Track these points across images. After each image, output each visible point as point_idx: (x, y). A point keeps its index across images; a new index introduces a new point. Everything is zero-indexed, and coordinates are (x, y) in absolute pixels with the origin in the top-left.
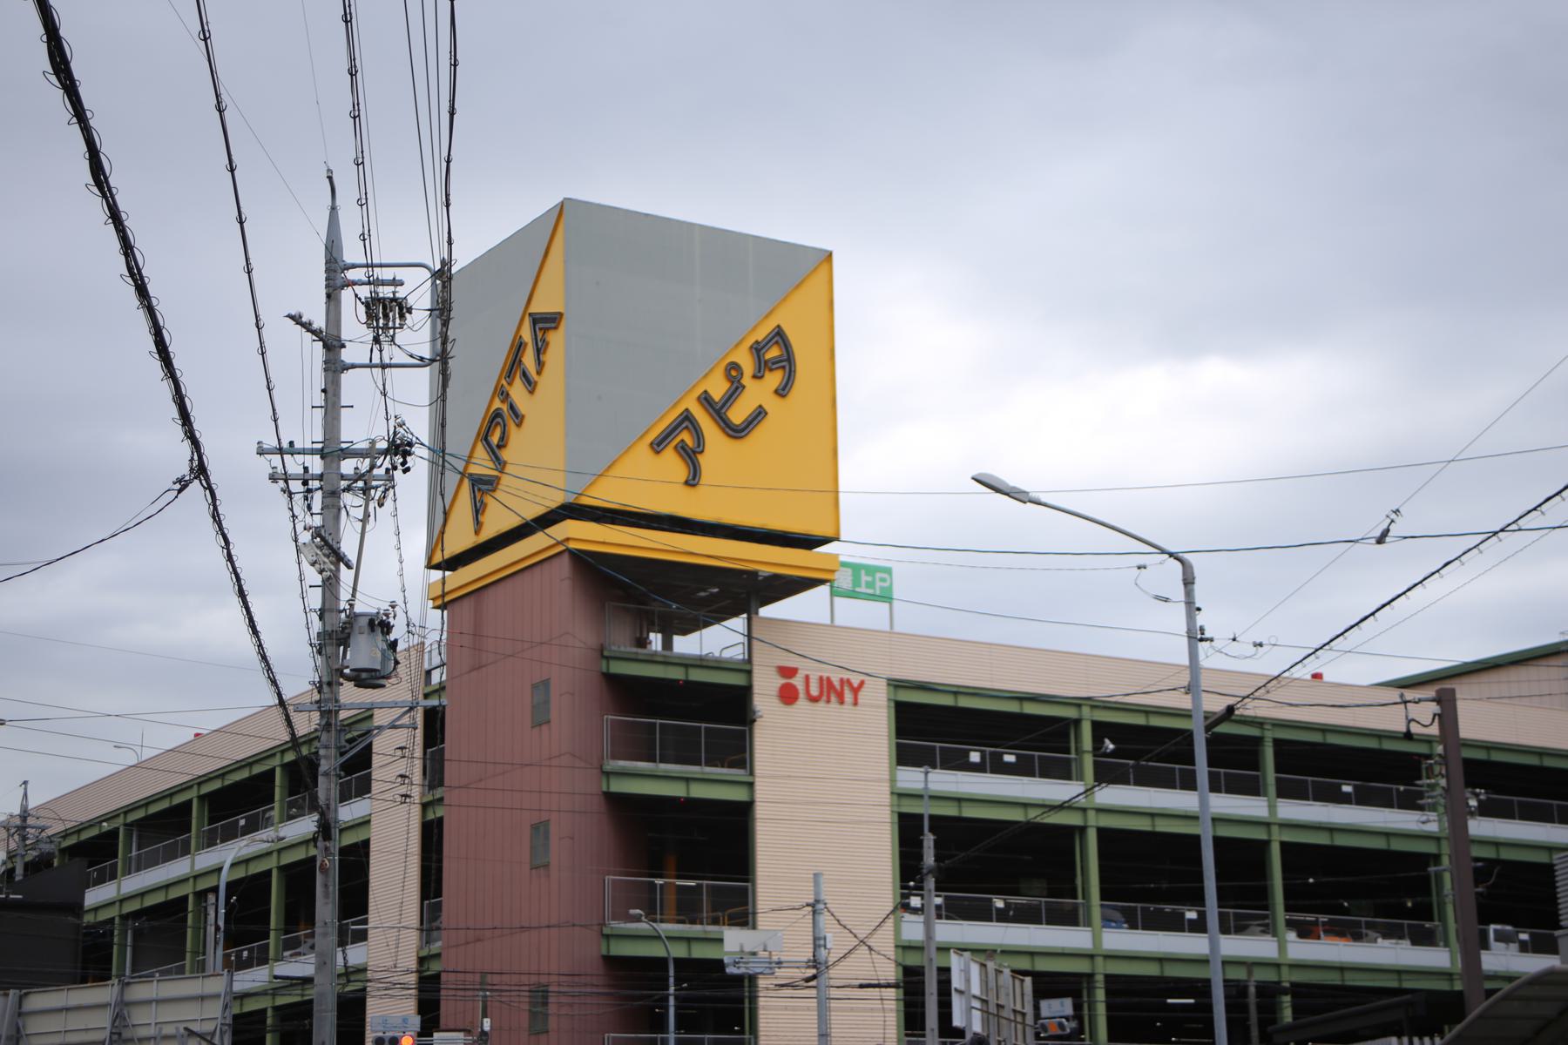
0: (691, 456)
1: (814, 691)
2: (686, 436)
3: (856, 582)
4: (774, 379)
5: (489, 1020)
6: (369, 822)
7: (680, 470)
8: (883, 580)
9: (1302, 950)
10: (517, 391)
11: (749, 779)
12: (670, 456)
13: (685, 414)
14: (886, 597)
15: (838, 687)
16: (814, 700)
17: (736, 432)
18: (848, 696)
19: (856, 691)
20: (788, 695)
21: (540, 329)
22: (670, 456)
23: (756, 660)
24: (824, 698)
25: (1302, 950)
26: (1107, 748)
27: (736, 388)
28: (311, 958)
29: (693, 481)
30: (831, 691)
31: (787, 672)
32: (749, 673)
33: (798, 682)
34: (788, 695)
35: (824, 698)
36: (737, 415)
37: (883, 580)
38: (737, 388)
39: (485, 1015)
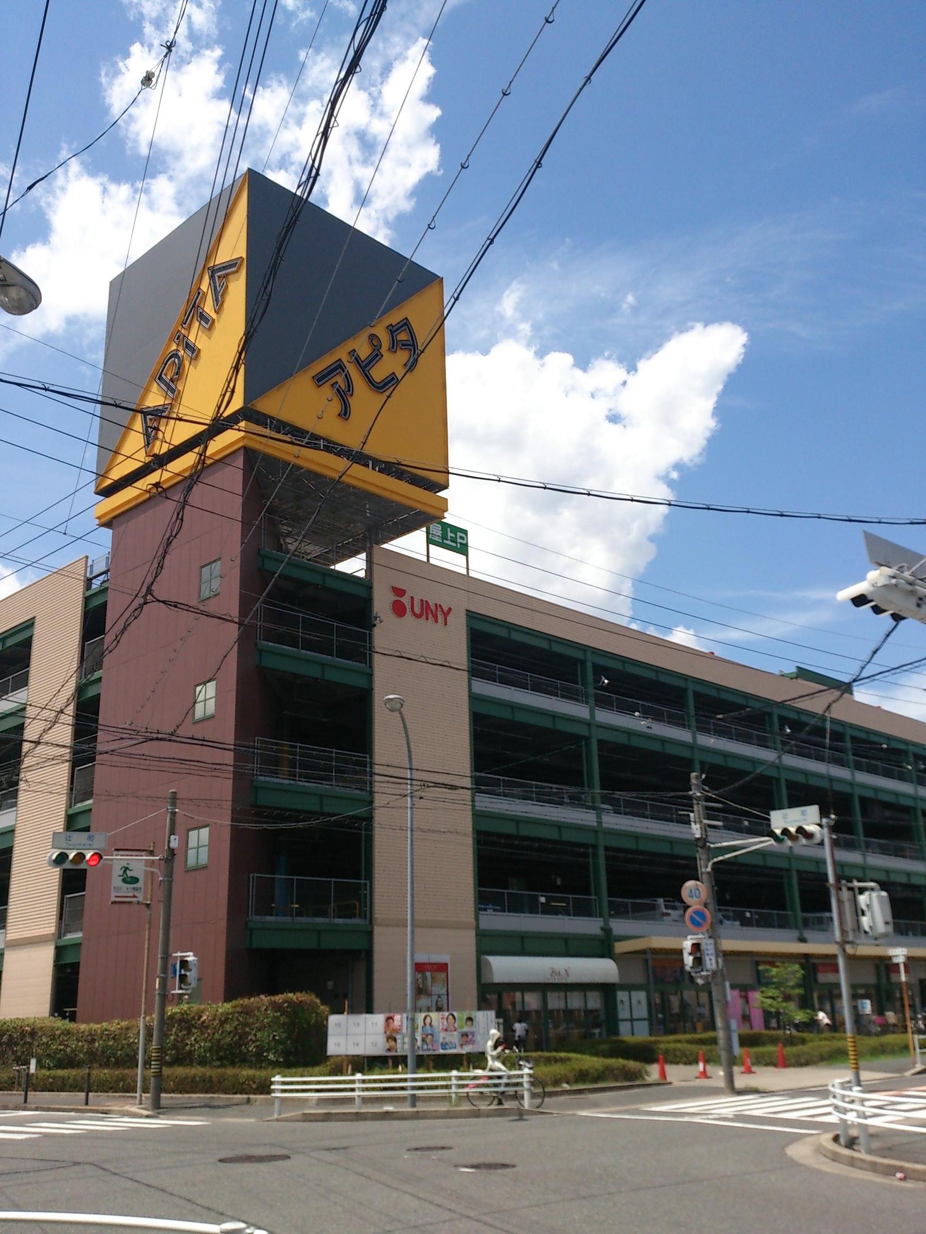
0: (344, 395)
1: (417, 610)
2: (340, 380)
3: (444, 537)
4: (403, 356)
5: (177, 837)
6: (13, 831)
7: (336, 406)
8: (461, 538)
9: (614, 821)
10: (195, 335)
11: (367, 670)
12: (327, 391)
13: (339, 363)
14: (463, 549)
15: (433, 608)
16: (418, 616)
17: (379, 387)
18: (440, 617)
19: (446, 614)
20: (399, 610)
21: (219, 277)
22: (327, 391)
23: (376, 576)
24: (424, 617)
25: (614, 821)
26: (604, 682)
27: (376, 356)
28: (881, 928)
29: (345, 413)
30: (429, 611)
31: (399, 592)
32: (371, 588)
33: (405, 600)
34: (399, 610)
35: (424, 617)
36: (379, 373)
37: (461, 538)
38: (377, 355)
39: (172, 832)
